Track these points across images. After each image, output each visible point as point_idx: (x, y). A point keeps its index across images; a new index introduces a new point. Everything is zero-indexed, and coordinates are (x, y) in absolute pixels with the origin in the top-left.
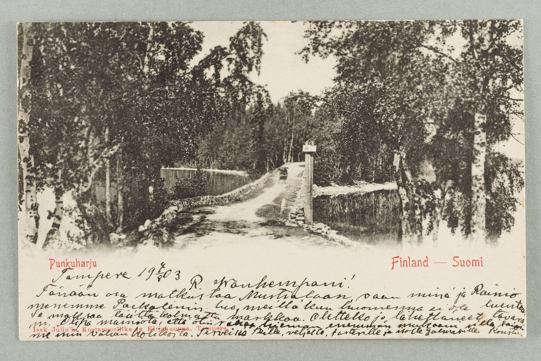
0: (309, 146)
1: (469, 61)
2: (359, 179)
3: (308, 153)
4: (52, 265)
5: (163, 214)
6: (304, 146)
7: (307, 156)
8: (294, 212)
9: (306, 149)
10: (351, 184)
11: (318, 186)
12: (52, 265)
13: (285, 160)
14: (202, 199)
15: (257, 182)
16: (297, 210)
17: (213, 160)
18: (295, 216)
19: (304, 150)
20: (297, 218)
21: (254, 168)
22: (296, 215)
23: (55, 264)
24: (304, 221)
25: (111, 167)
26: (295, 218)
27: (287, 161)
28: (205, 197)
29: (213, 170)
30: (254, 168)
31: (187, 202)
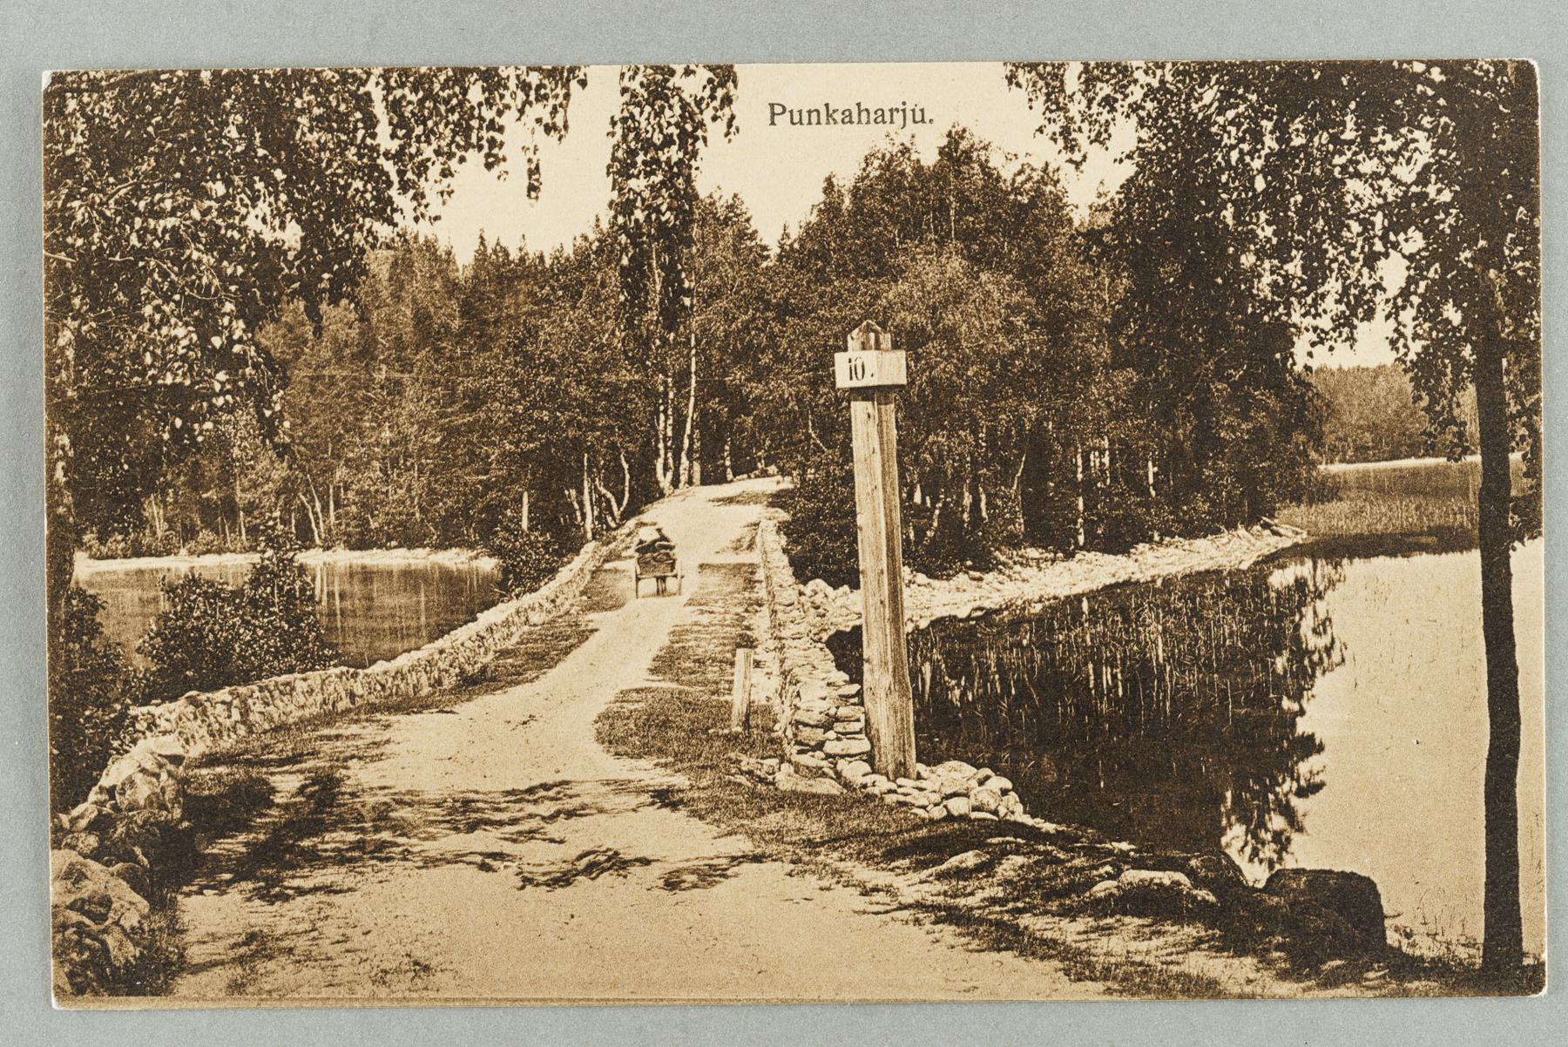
0: (870, 357)
1: (1037, 220)
2: (1014, 542)
3: (865, 393)
5: (106, 781)
6: (840, 359)
7: (859, 409)
8: (814, 717)
9: (852, 373)
10: (984, 564)
11: (835, 587)
13: (665, 482)
14: (301, 686)
15: (547, 589)
16: (824, 705)
17: (325, 508)
18: (819, 734)
19: (843, 381)
20: (831, 747)
21: (525, 524)
22: (827, 727)
24: (870, 758)
25: (520, 833)
26: (820, 746)
27: (675, 483)
28: (315, 677)
29: (328, 557)
30: (525, 524)
31: (229, 705)
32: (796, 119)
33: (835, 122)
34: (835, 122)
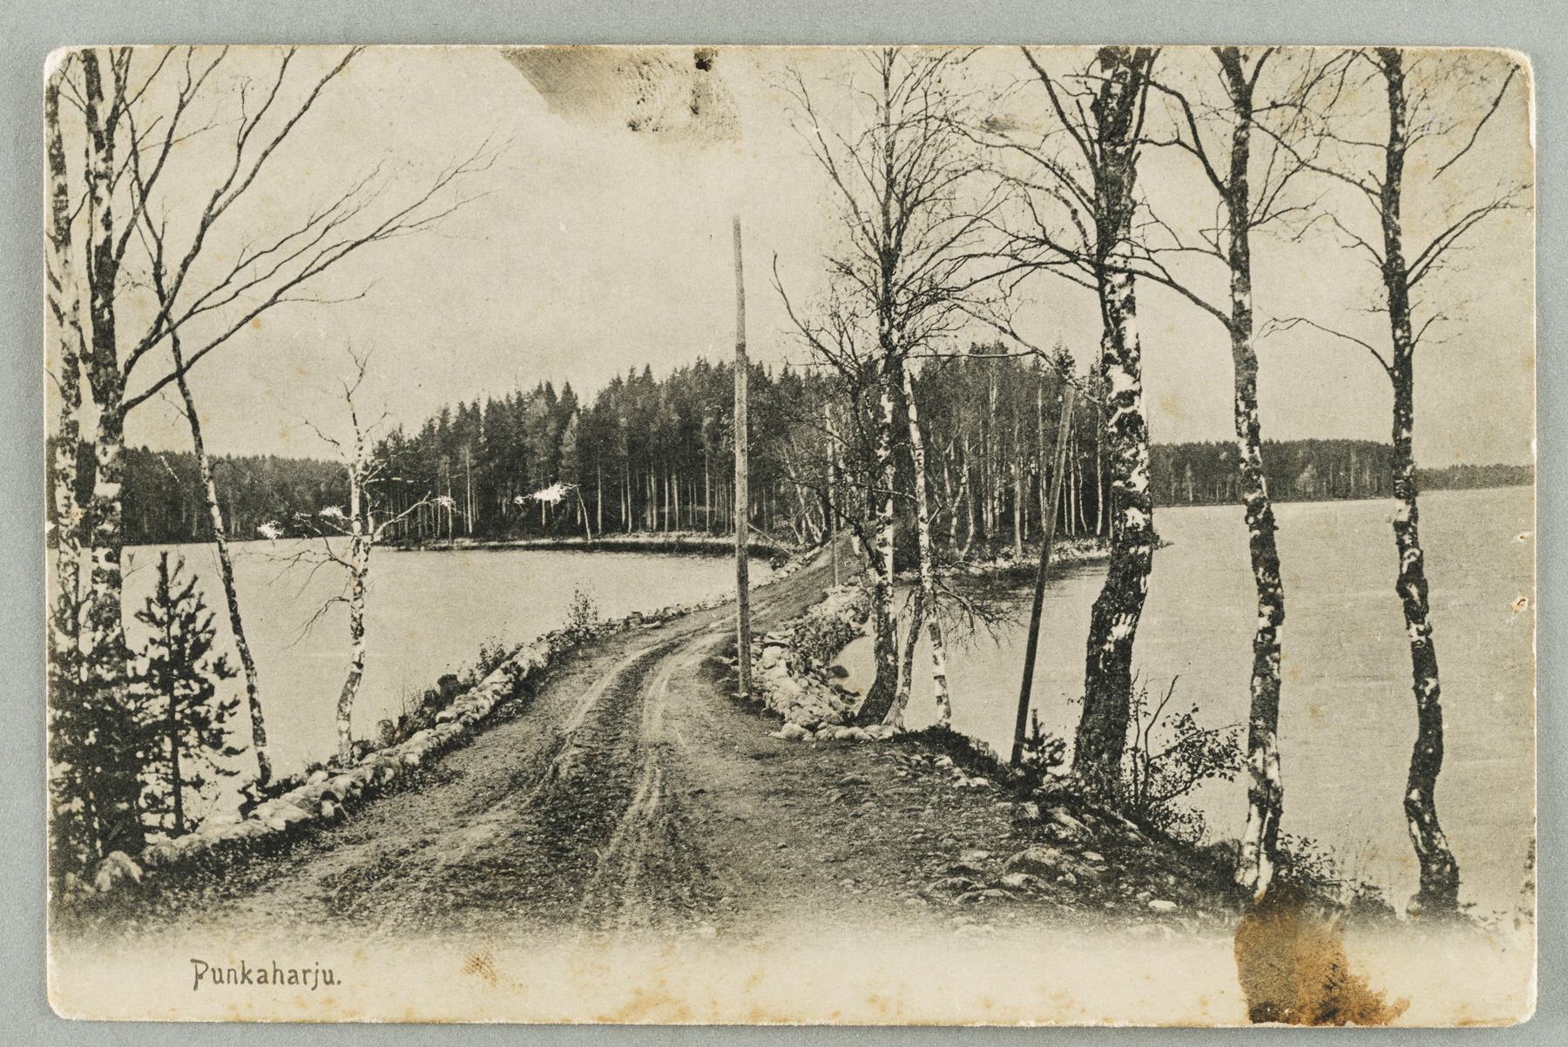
4: (199, 976)
12: (199, 976)
23: (209, 975)
32: (218, 979)
33: (251, 982)
34: (251, 982)
